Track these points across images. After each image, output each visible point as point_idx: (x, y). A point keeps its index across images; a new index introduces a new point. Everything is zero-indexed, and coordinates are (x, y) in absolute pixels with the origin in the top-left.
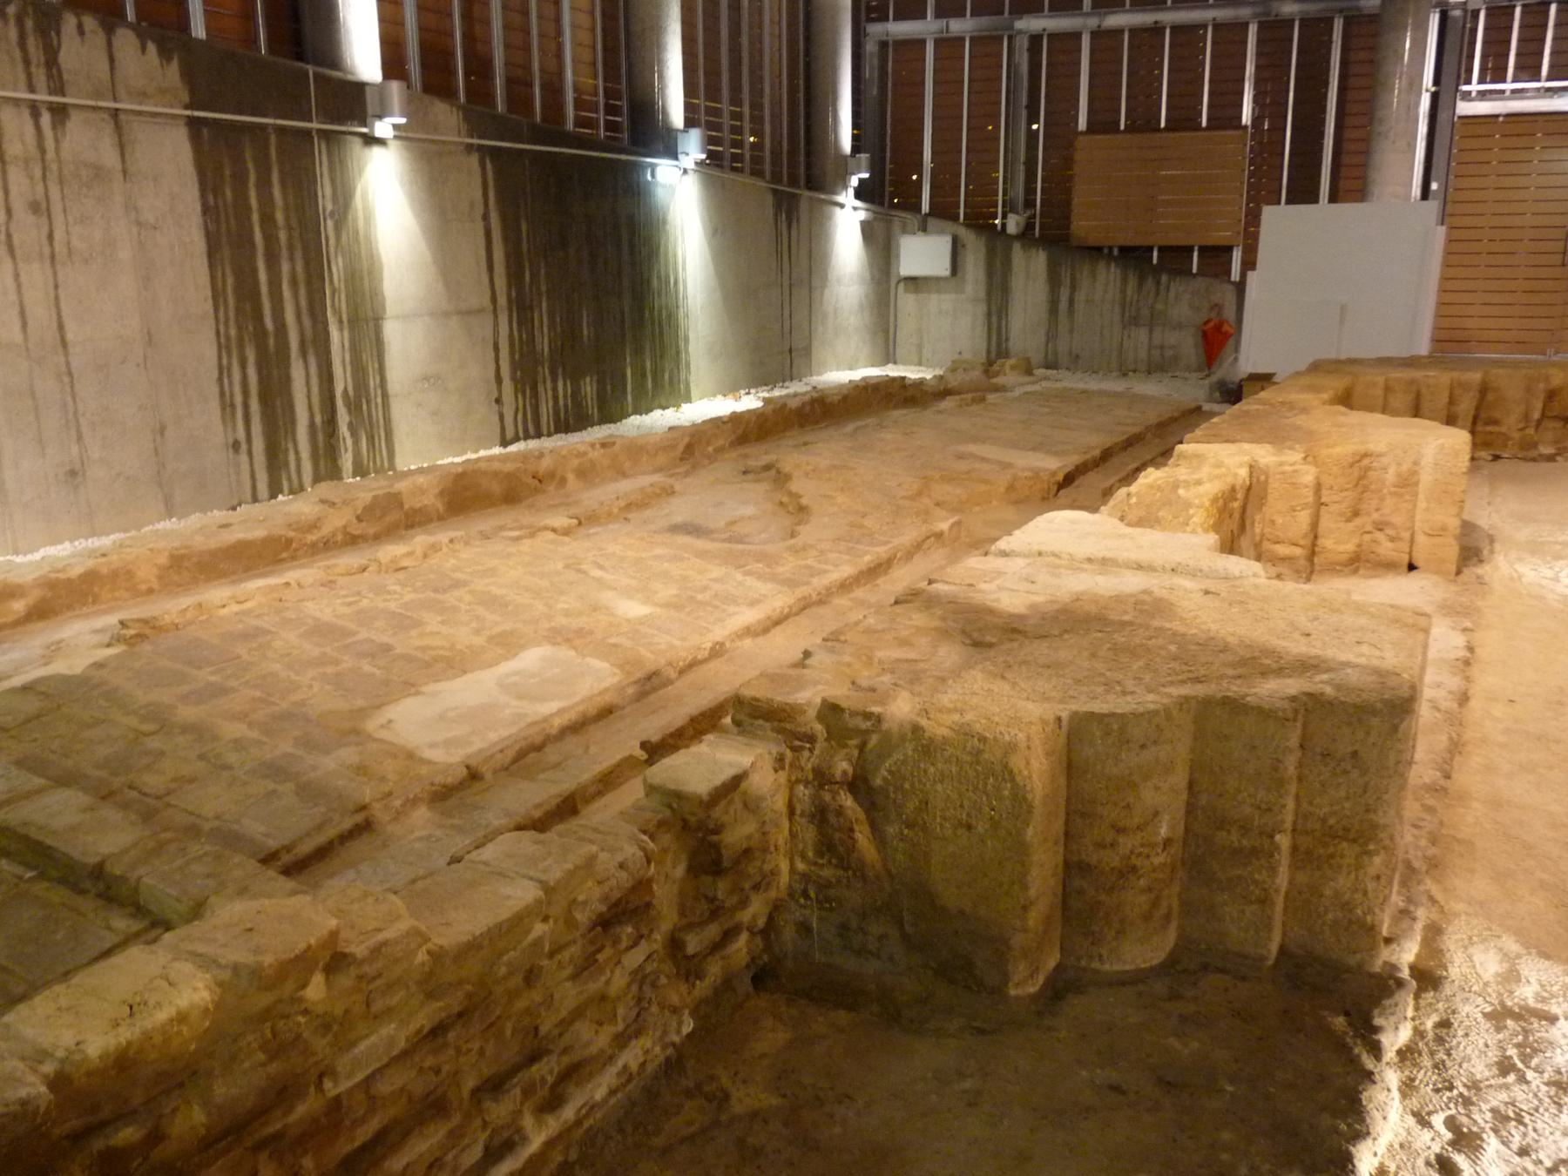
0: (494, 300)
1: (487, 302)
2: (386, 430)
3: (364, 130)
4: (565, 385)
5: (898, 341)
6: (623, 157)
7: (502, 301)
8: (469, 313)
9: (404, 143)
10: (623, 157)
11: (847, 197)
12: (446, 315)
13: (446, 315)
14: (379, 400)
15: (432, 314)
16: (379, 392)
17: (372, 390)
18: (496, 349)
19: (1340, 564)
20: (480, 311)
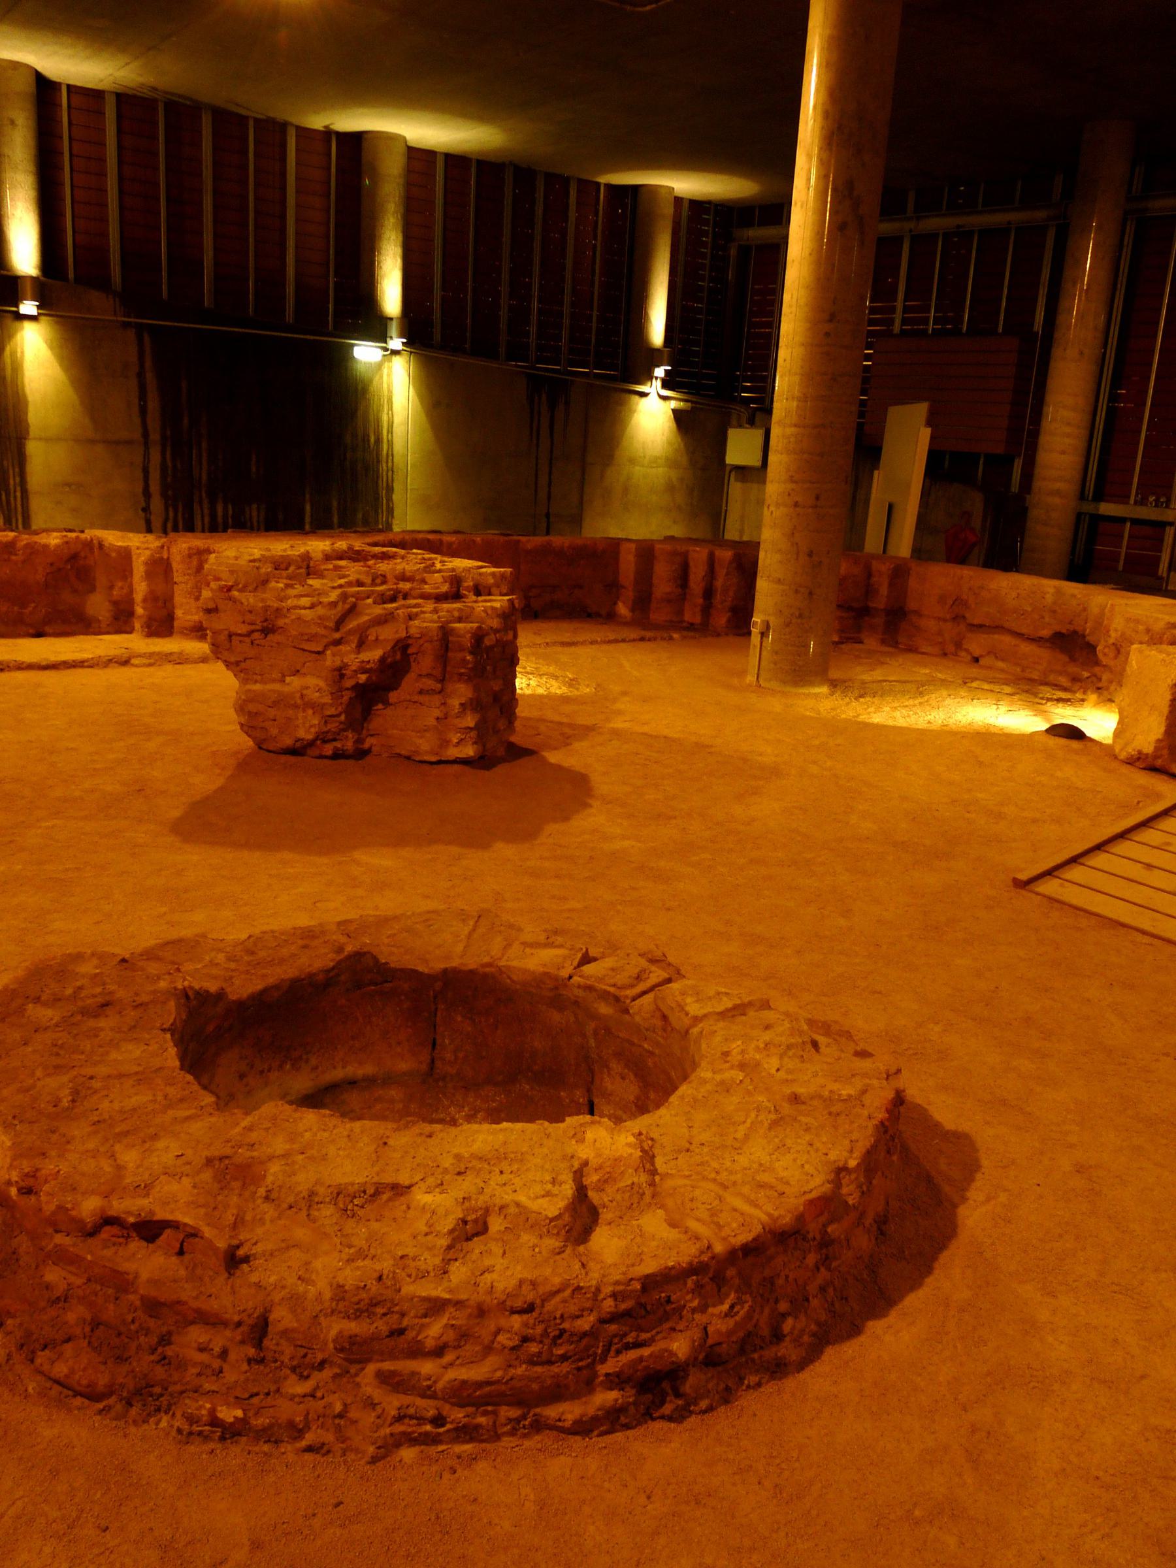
0: (146, 435)
1: (137, 435)
2: (23, 516)
3: (14, 309)
4: (225, 509)
5: (727, 527)
6: (330, 339)
7: (155, 436)
8: (117, 443)
9: (55, 319)
10: (330, 339)
11: (654, 388)
12: (92, 442)
13: (92, 442)
14: (18, 494)
15: (77, 440)
16: (18, 489)
17: (12, 487)
18: (146, 471)
19: (186, 629)
20: (129, 442)
